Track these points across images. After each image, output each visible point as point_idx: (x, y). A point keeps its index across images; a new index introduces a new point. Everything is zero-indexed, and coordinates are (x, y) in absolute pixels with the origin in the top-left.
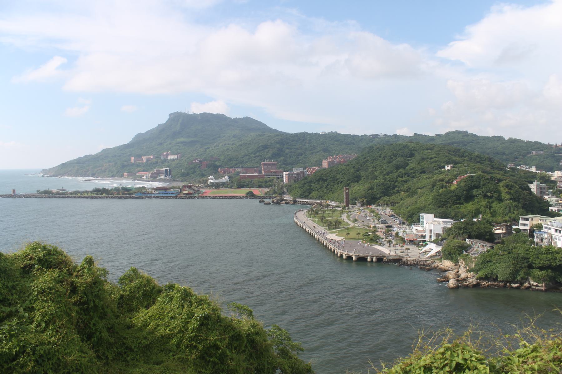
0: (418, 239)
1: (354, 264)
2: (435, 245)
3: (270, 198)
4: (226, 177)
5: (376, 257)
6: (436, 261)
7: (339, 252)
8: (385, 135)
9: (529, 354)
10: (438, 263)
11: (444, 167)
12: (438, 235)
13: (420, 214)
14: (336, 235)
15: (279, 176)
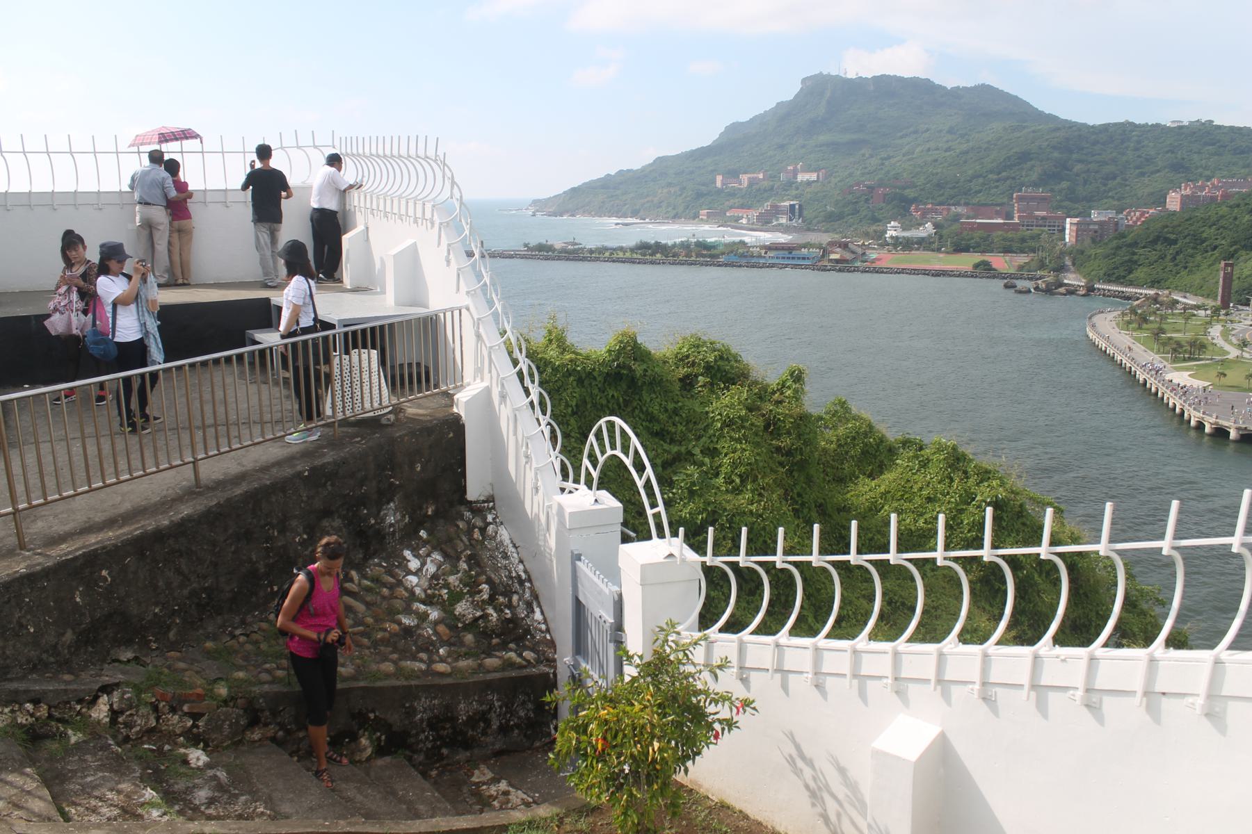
7: (1194, 416)
15: (1054, 226)
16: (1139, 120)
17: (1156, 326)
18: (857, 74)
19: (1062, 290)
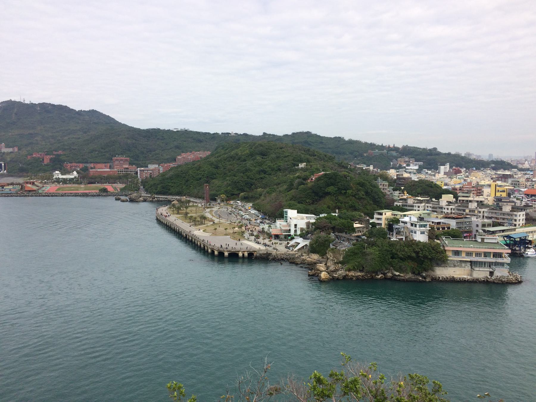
0: (283, 234)
1: (226, 260)
2: (301, 239)
3: (126, 196)
4: (75, 173)
5: (247, 252)
6: (303, 254)
8: (236, 134)
9: (16, 308)
10: (305, 257)
11: (298, 165)
12: (302, 230)
13: (284, 210)
14: (203, 231)
15: (132, 171)
16: (162, 128)
17: (185, 211)
18: (30, 102)
19: (141, 199)
